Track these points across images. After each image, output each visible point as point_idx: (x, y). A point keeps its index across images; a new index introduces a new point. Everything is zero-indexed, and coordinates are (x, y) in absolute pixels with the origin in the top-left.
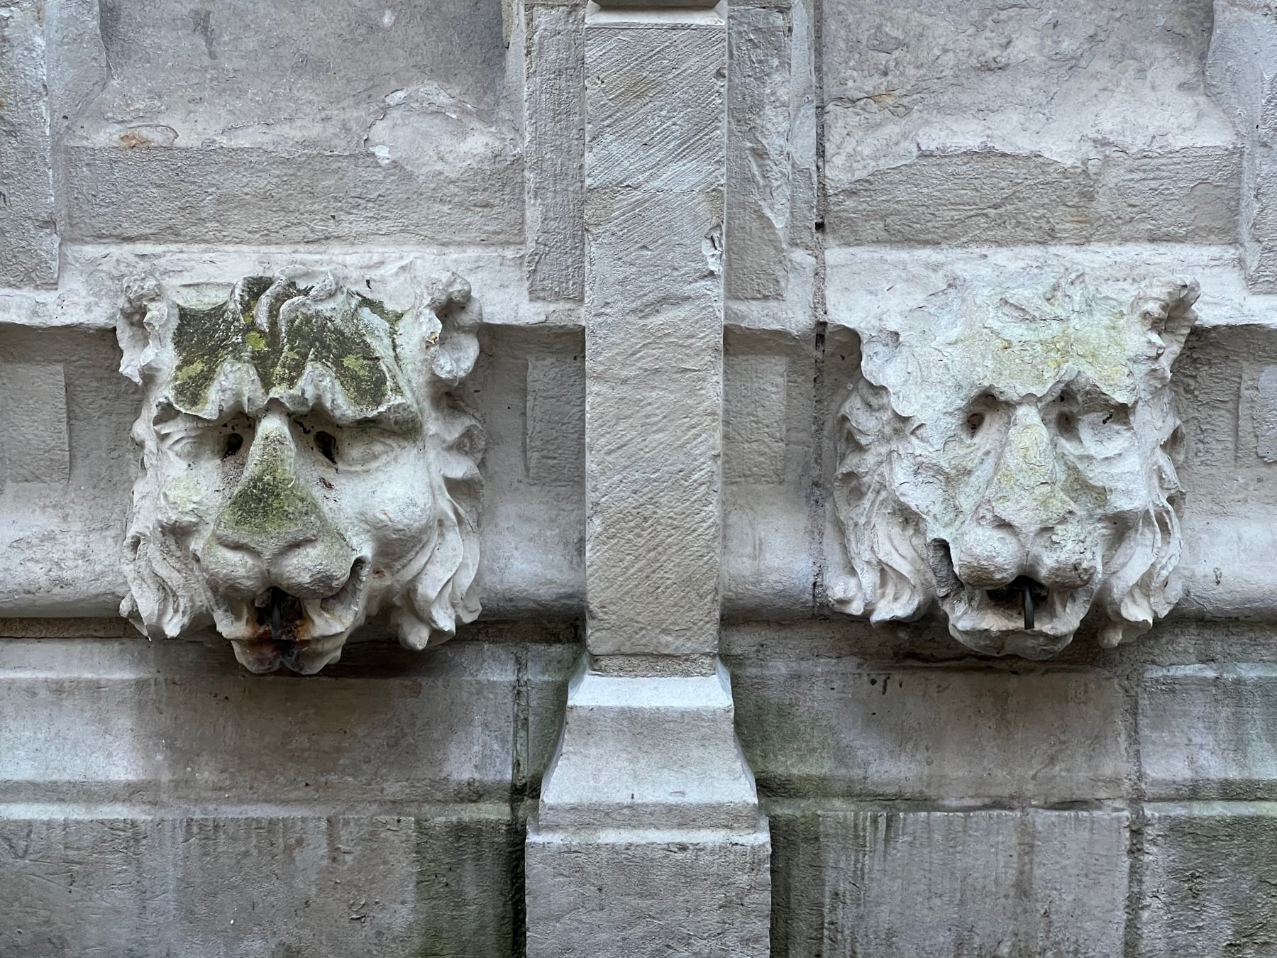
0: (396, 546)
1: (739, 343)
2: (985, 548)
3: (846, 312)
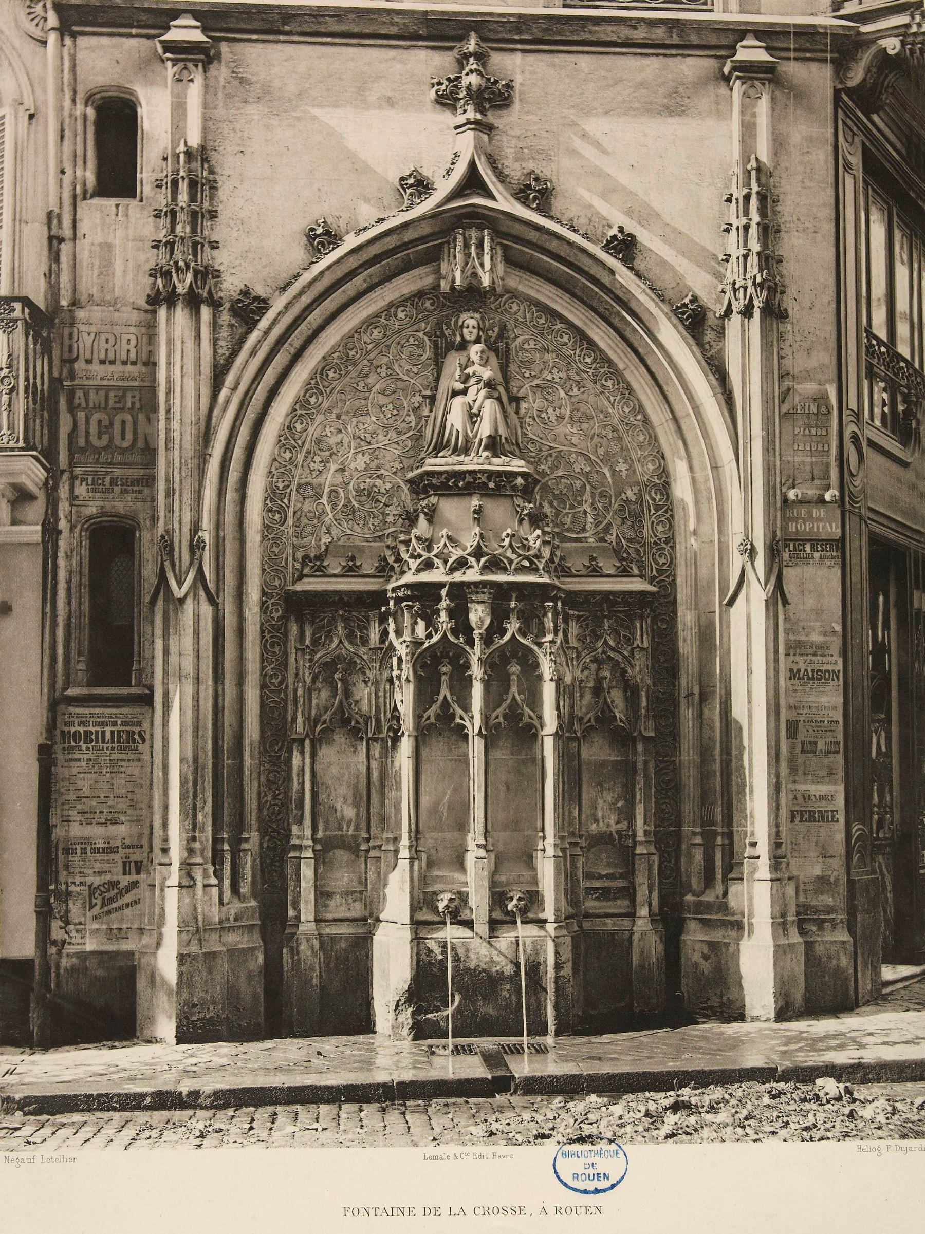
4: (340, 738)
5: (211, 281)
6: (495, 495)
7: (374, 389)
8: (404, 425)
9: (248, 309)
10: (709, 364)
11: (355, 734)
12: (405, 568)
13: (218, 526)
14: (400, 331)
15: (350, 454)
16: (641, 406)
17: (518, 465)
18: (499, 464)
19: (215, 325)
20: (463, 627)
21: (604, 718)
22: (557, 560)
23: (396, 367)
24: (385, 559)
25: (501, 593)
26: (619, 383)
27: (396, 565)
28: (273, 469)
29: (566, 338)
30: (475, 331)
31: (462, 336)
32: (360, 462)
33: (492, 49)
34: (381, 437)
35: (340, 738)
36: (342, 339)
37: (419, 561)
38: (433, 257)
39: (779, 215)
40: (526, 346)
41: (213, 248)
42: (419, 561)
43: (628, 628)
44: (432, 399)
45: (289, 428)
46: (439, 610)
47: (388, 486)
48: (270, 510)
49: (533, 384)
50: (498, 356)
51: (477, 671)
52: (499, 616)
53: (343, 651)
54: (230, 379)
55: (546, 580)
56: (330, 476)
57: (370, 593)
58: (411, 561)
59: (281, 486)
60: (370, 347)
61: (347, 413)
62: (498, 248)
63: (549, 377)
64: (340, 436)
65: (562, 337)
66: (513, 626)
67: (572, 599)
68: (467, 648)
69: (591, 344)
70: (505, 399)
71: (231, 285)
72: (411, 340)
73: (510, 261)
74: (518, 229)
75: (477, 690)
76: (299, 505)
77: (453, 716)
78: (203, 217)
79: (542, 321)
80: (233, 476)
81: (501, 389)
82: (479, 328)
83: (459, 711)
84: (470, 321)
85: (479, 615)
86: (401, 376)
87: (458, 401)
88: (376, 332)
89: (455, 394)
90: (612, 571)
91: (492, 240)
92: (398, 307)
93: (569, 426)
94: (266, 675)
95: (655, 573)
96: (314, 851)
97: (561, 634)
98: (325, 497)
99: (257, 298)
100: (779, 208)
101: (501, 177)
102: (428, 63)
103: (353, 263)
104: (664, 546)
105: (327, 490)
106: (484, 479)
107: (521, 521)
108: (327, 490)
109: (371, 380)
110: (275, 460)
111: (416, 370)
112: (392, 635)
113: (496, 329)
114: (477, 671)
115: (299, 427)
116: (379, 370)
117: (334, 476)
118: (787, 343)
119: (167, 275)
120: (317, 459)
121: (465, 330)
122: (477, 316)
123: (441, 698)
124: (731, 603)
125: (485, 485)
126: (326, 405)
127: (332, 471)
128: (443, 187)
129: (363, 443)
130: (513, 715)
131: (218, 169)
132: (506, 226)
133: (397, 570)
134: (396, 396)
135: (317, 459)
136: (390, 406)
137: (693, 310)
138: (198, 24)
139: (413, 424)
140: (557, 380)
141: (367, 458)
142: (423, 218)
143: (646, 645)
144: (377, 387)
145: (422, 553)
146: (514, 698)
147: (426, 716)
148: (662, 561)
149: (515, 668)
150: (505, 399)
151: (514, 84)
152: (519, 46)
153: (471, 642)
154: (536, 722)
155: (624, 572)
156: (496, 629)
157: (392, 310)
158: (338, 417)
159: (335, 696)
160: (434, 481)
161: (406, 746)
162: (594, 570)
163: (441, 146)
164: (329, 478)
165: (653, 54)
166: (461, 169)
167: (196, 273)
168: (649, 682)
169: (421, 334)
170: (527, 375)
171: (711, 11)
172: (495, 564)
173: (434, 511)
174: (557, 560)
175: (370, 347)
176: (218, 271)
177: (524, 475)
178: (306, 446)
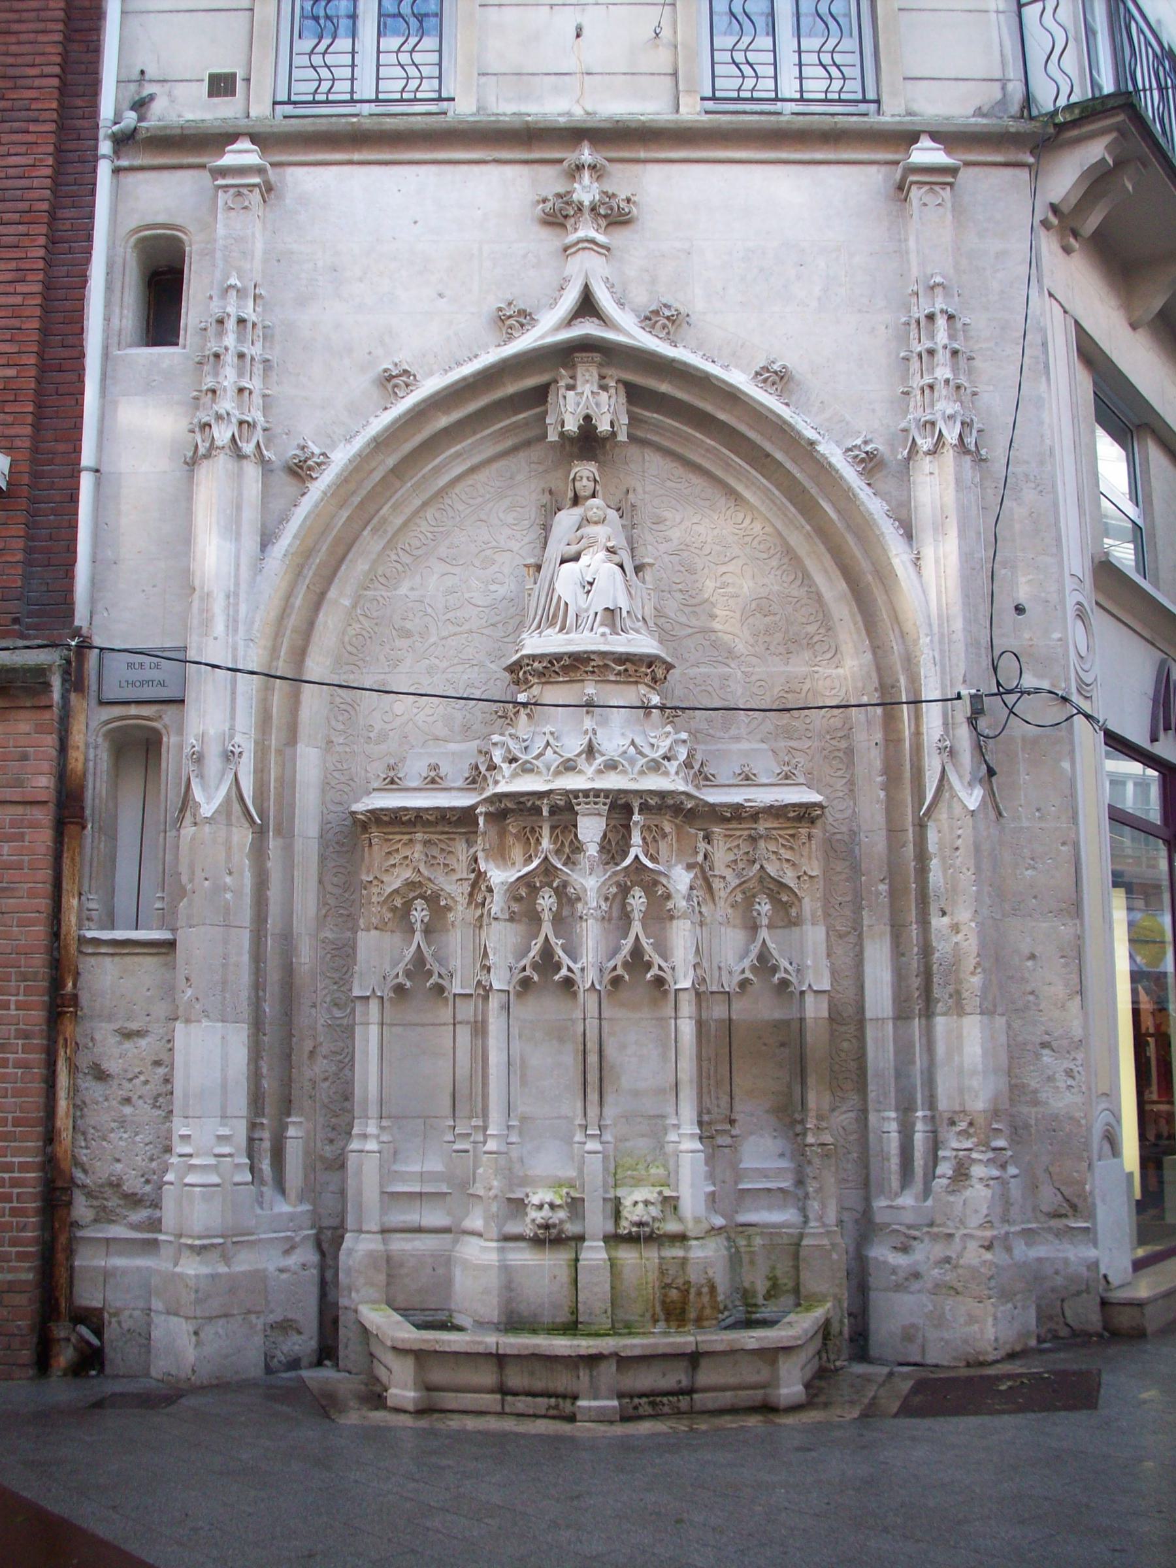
0: (562, 1222)
1: (605, 1199)
2: (636, 1219)
3: (619, 1195)
24: (477, 768)
27: (488, 774)
70: (629, 567)
80: (593, 1059)
130: (547, 961)
137: (867, 453)
150: (629, 567)
155: (787, 778)
162: (747, 778)
174: (697, 766)
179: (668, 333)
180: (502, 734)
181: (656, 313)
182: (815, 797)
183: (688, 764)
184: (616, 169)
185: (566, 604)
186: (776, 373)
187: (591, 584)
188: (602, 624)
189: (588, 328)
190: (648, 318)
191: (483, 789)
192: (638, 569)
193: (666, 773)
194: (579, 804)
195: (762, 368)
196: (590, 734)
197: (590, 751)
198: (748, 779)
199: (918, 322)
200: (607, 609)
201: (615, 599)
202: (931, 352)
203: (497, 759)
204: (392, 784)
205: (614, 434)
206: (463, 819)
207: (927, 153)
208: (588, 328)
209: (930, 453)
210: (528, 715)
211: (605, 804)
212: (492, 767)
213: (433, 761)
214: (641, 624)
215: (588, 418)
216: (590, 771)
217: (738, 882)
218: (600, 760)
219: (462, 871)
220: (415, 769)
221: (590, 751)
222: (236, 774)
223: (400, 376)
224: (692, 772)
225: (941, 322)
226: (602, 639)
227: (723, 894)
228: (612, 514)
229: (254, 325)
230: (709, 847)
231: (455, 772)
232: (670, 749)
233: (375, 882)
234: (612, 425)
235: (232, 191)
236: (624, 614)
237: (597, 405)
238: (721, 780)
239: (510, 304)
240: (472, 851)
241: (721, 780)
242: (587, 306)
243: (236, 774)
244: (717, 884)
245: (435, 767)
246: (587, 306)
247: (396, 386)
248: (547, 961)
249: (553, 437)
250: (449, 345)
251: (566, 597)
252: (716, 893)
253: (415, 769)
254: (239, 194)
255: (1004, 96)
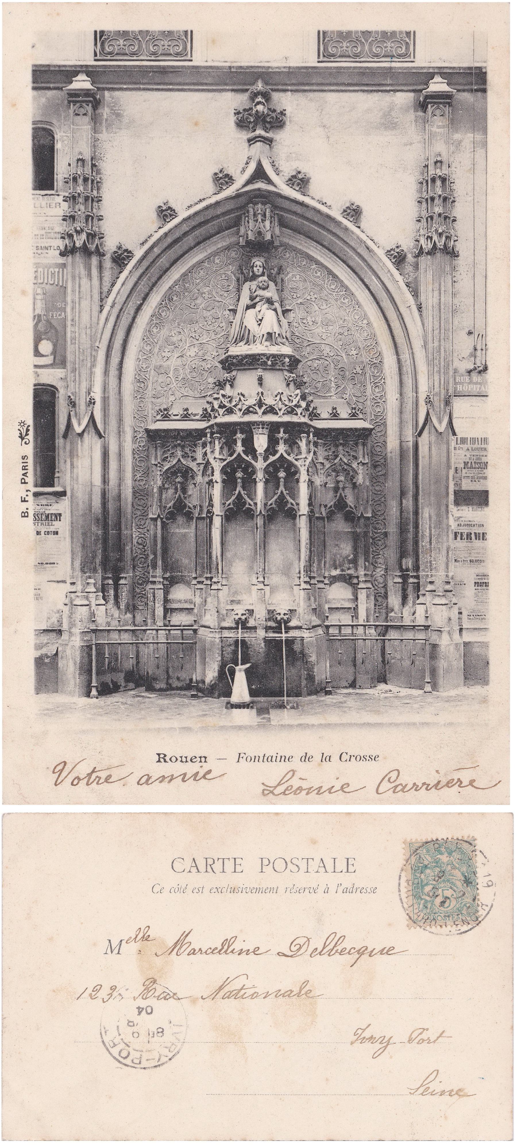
4: (180, 520)
5: (97, 241)
6: (273, 368)
7: (201, 307)
8: (219, 329)
9: (121, 258)
10: (407, 286)
11: (189, 516)
12: (217, 415)
13: (105, 389)
14: (216, 271)
15: (186, 348)
16: (366, 315)
17: (286, 350)
18: (274, 350)
19: (101, 267)
20: (249, 448)
21: (341, 504)
22: (311, 409)
23: (214, 293)
24: (206, 410)
25: (273, 428)
26: (352, 300)
27: (212, 413)
28: (140, 357)
29: (319, 274)
30: (261, 269)
31: (253, 272)
32: (192, 352)
33: (272, 90)
34: (205, 336)
35: (180, 520)
36: (181, 276)
37: (224, 409)
38: (237, 223)
39: (455, 192)
40: (294, 279)
41: (100, 220)
42: (224, 409)
43: (356, 451)
44: (234, 311)
45: (149, 331)
46: (235, 440)
47: (209, 366)
48: (139, 381)
49: (299, 302)
50: (276, 285)
51: (260, 475)
52: (273, 442)
53: (180, 465)
54: (110, 300)
55: (303, 420)
56: (174, 360)
57: (196, 430)
58: (220, 410)
59: (144, 367)
60: (198, 281)
61: (185, 322)
62: (276, 216)
63: (309, 298)
64: (180, 336)
65: (316, 273)
66: (282, 448)
67: (319, 433)
68: (253, 462)
69: (335, 276)
70: (279, 311)
71: (110, 245)
72: (223, 276)
73: (283, 224)
74: (286, 204)
75: (260, 487)
76: (155, 379)
77: (245, 503)
78: (93, 200)
79: (304, 263)
80: (115, 360)
81: (277, 305)
82: (264, 268)
83: (249, 501)
84: (258, 262)
85: (261, 442)
86: (217, 299)
87: (251, 311)
88: (202, 272)
89: (248, 307)
90: (346, 416)
91: (272, 211)
92: (215, 256)
93: (321, 328)
94: (136, 480)
95: (373, 417)
96: (163, 585)
97: (312, 454)
98: (171, 372)
99: (126, 250)
100: (454, 187)
101: (277, 172)
102: (231, 101)
103: (185, 228)
104: (379, 401)
105: (172, 369)
106: (265, 359)
107: (288, 385)
108: (172, 369)
109: (198, 301)
110: (141, 351)
111: (226, 295)
112: (209, 455)
113: (276, 269)
114: (260, 475)
115: (155, 330)
116: (204, 295)
117: (176, 361)
118: (458, 273)
119: (70, 236)
120: (166, 350)
121: (255, 269)
122: (263, 260)
123: (237, 492)
124: (420, 434)
125: (265, 363)
126: (171, 318)
127: (175, 358)
128: (240, 180)
129: (194, 340)
130: (281, 501)
131: (102, 171)
132: (279, 201)
133: (213, 416)
134: (214, 311)
135: (166, 350)
136: (210, 318)
137: (398, 253)
138: (89, 79)
139: (224, 328)
140: (314, 300)
141: (196, 349)
142: (228, 199)
143: (367, 461)
144: (203, 305)
145: (227, 404)
146: (282, 492)
147: (228, 503)
148: (378, 410)
149: (282, 474)
150: (279, 311)
151: (286, 112)
152: (289, 88)
153: (255, 458)
154: (295, 507)
155: (353, 416)
156: (271, 449)
157: (212, 258)
158: (179, 325)
159: (176, 493)
160: (234, 361)
161: (217, 522)
162: (335, 415)
163: (235, 153)
164: (174, 362)
165: (375, 91)
166: (252, 167)
167: (88, 235)
168: (368, 484)
169: (229, 273)
170: (295, 297)
171: (191, 61)
172: (271, 410)
173: (234, 379)
174: (311, 409)
175: (198, 281)
176: (103, 234)
177: (290, 357)
178: (160, 342)
179: (300, 188)
180: (218, 394)
181: (294, 177)
182: (367, 425)
183: (307, 409)
184: (275, 96)
185: (249, 331)
186: (354, 210)
187: (261, 320)
188: (266, 341)
189: (260, 185)
190: (290, 180)
191: (209, 420)
192: (285, 312)
193: (297, 414)
194: (254, 429)
195: (347, 208)
196: (260, 395)
197: (260, 404)
198: (335, 415)
199: (427, 181)
200: (268, 333)
201: (272, 327)
202: (433, 199)
203: (216, 406)
204: (166, 417)
205: (273, 242)
206: (200, 433)
207: (438, 85)
208: (260, 185)
209: (428, 253)
210: (230, 385)
211: (267, 428)
212: (213, 410)
213: (185, 407)
214: (285, 340)
215: (260, 233)
216: (260, 412)
217: (329, 465)
218: (264, 407)
219: (200, 460)
220: (177, 410)
221: (260, 404)
222: (92, 413)
223: (167, 210)
224: (308, 413)
225: (439, 183)
226: (266, 348)
227: (322, 472)
228: (272, 284)
229: (93, 181)
230: (316, 449)
231: (197, 409)
232: (298, 402)
233: (159, 465)
234: (272, 237)
235: (78, 105)
236: (277, 335)
237: (264, 226)
238: (323, 416)
239: (221, 171)
240: (205, 450)
241: (323, 416)
242: (260, 174)
243: (92, 413)
244: (319, 466)
245: (187, 410)
246: (260, 174)
247: (165, 215)
248: (281, 501)
249: (242, 242)
250: (191, 191)
251: (248, 327)
252: (319, 471)
253: (177, 410)
254: (81, 107)
255: (138, 663)
